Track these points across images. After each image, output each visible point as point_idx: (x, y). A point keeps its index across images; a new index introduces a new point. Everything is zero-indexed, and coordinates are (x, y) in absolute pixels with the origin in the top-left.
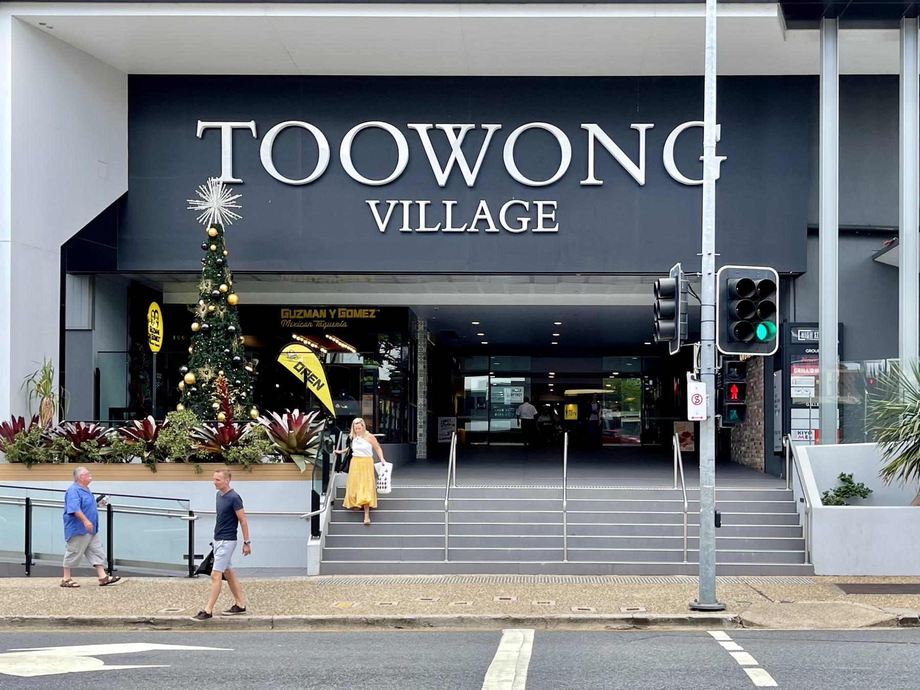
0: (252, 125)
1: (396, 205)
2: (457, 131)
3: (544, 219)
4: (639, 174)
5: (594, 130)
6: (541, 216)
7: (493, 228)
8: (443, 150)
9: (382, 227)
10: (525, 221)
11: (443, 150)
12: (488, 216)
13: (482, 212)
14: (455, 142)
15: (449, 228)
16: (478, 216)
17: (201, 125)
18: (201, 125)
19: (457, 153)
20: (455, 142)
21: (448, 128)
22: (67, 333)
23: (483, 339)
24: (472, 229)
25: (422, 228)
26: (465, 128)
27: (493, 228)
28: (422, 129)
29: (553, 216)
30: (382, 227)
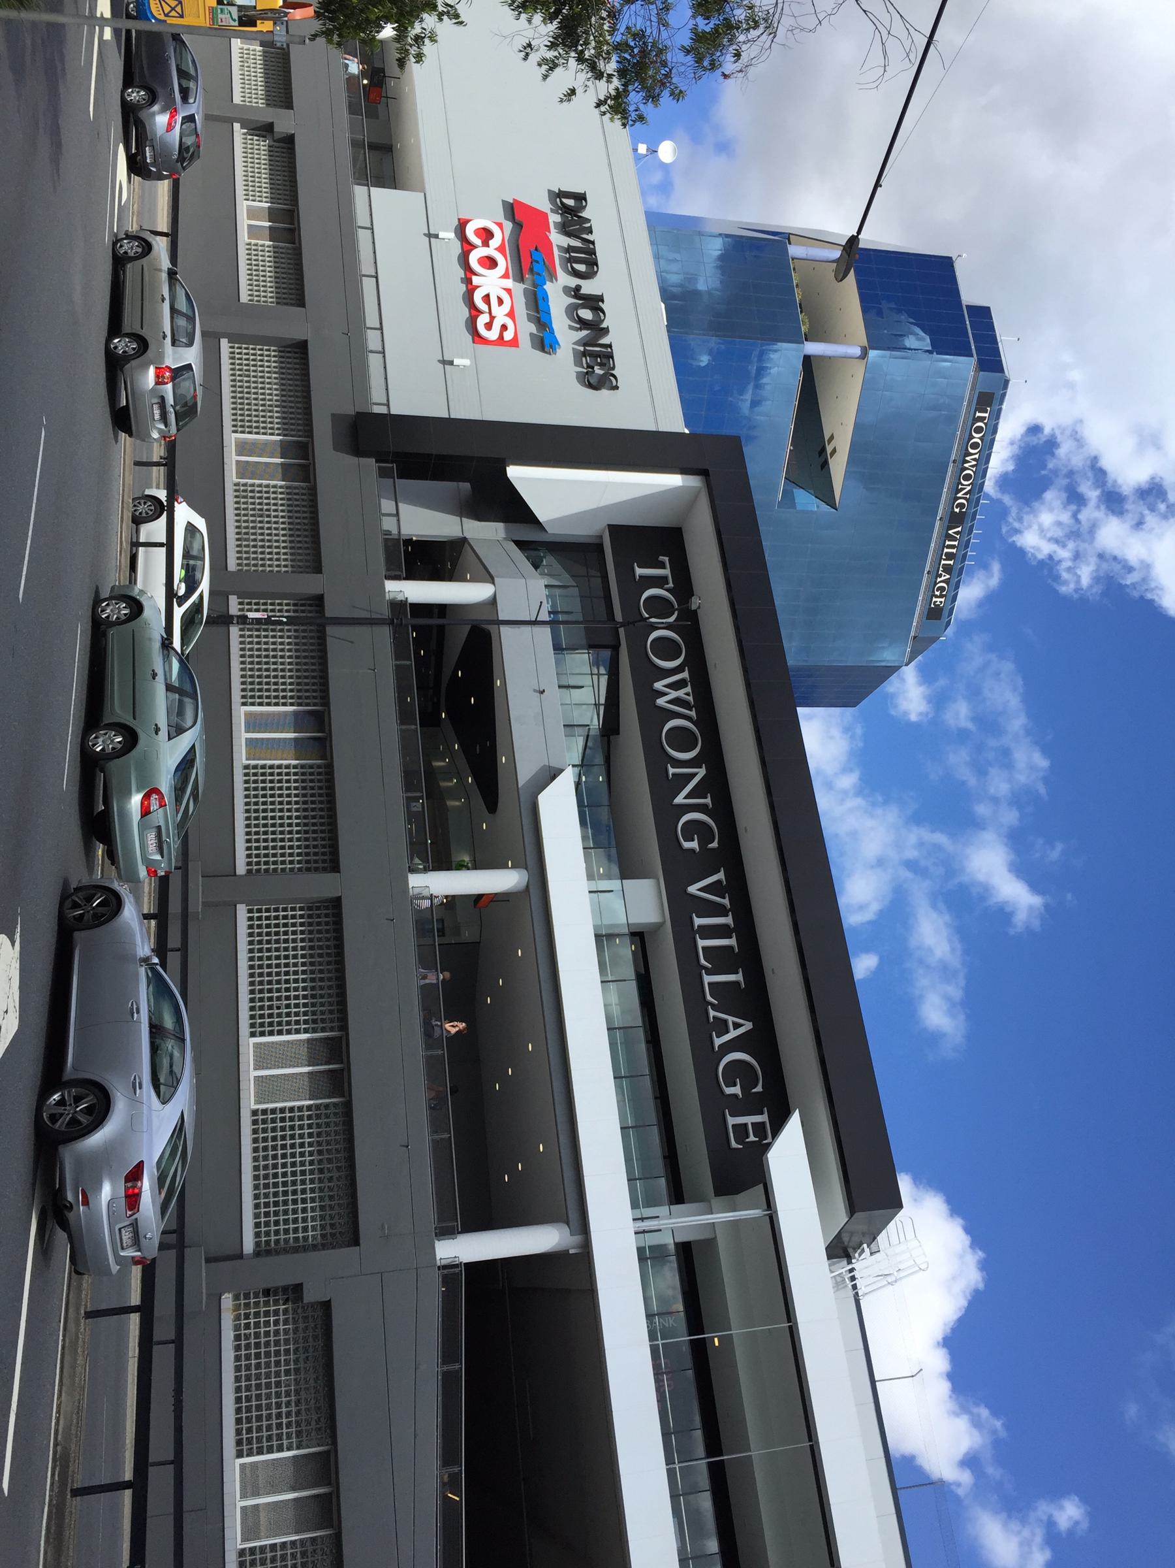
0: (671, 585)
1: (723, 906)
2: (688, 694)
3: (746, 1125)
4: (679, 799)
5: (701, 772)
6: (749, 1120)
7: (718, 1042)
8: (672, 686)
9: (693, 889)
10: (736, 1090)
11: (675, 686)
12: (733, 1034)
13: (737, 1026)
14: (680, 693)
15: (707, 979)
16: (731, 1019)
17: (666, 559)
18: (666, 559)
19: (674, 694)
20: (680, 693)
21: (688, 689)
22: (164, 541)
23: (513, 1172)
24: (712, 1013)
25: (702, 943)
26: (691, 698)
27: (718, 1042)
28: (685, 675)
29: (752, 1138)
30: (693, 889)
